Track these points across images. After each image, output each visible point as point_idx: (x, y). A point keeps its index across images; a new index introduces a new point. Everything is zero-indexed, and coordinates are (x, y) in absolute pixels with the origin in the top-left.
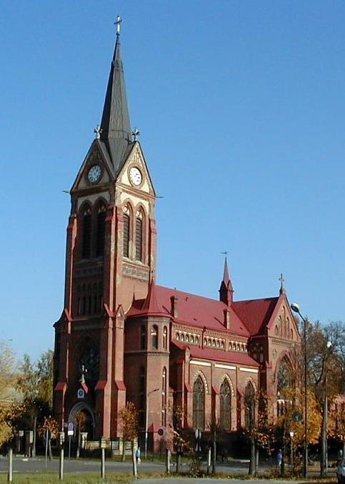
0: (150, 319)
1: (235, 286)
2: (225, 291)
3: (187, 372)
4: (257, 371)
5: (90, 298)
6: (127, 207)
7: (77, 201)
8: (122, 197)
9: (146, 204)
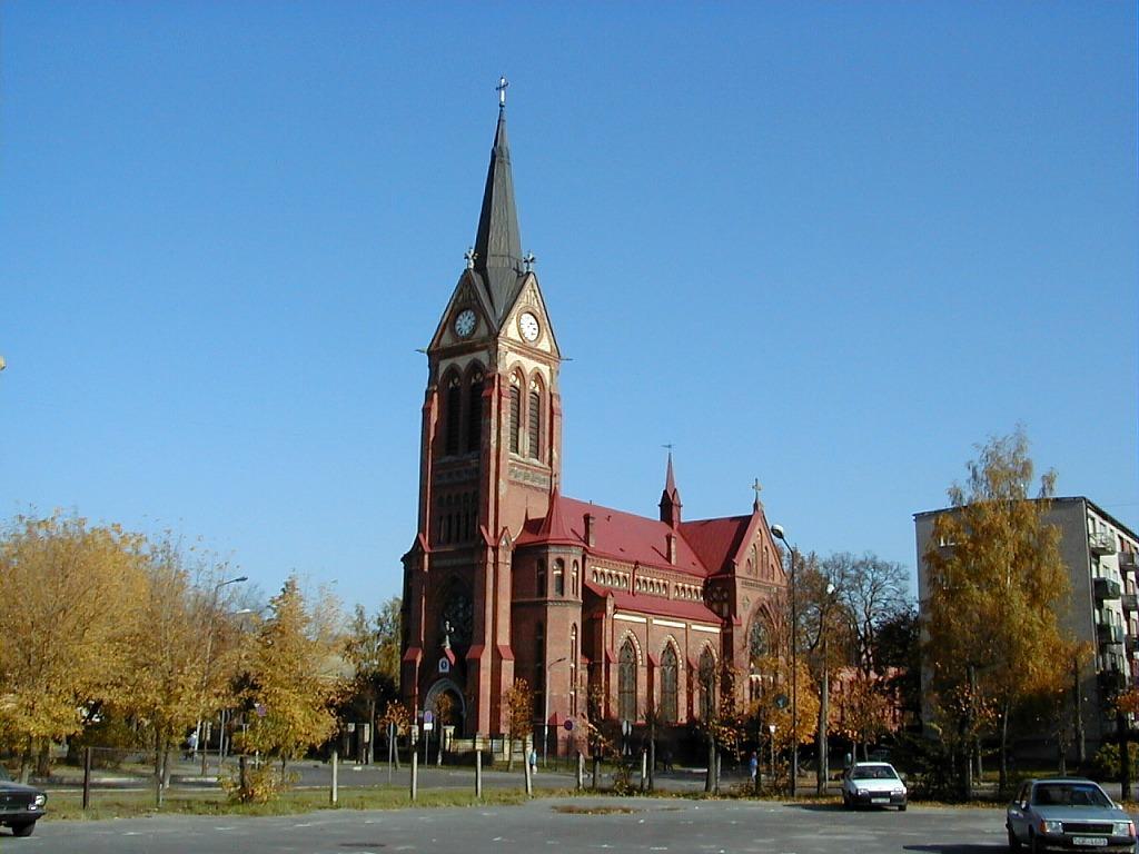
0: (552, 550)
1: (683, 497)
2: (668, 505)
3: (609, 632)
4: (718, 630)
5: (458, 516)
6: (517, 376)
7: (437, 366)
8: (509, 360)
9: (545, 370)
